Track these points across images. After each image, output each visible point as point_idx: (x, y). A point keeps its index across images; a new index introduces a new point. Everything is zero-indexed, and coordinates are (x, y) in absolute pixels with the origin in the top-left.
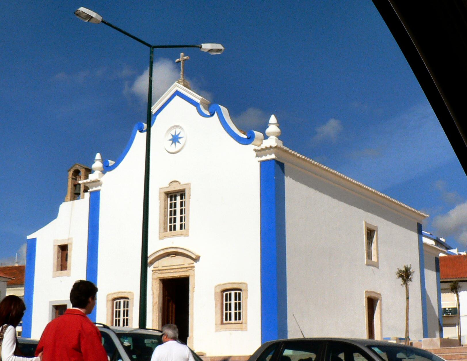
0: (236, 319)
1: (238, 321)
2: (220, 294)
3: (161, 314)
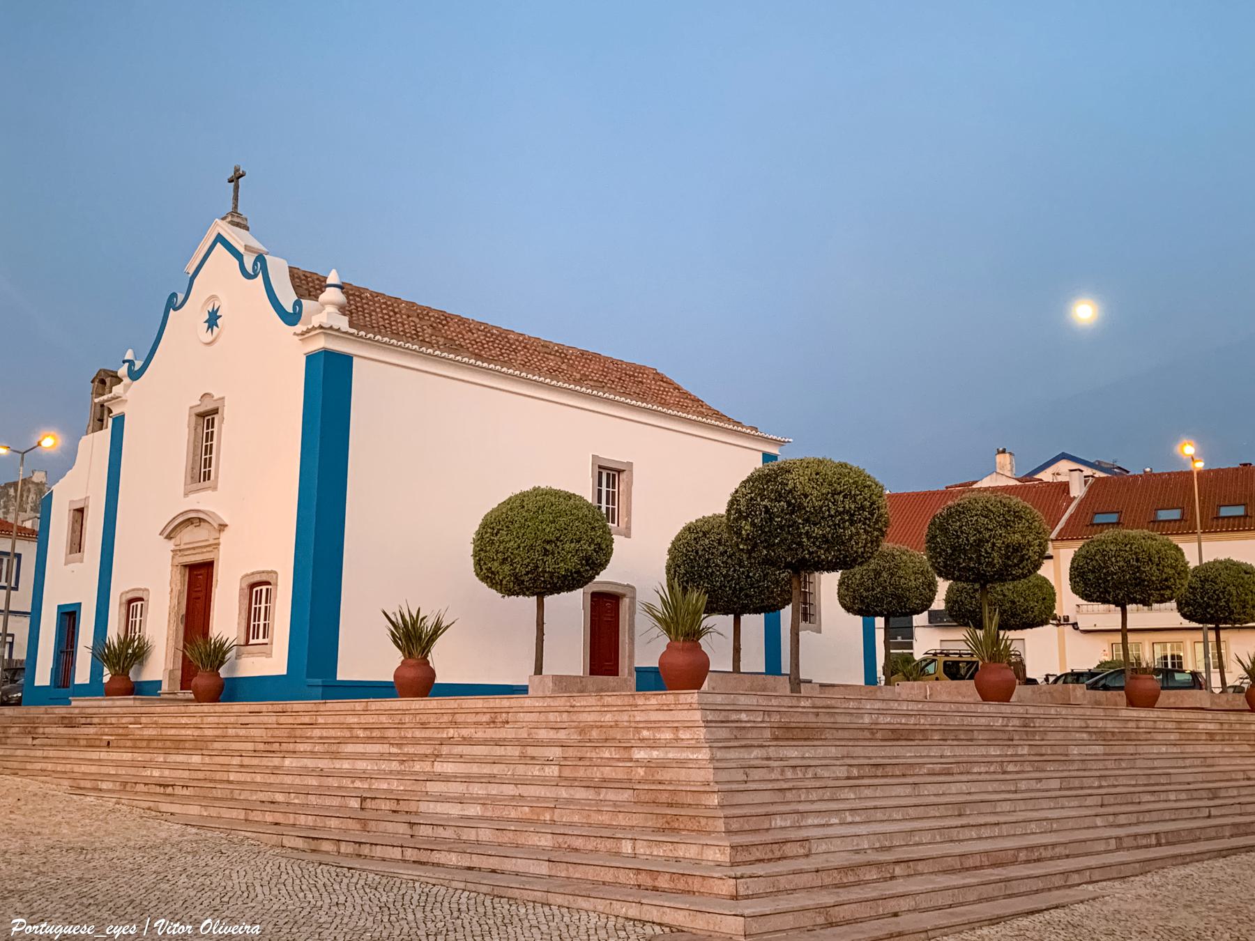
2: (247, 591)
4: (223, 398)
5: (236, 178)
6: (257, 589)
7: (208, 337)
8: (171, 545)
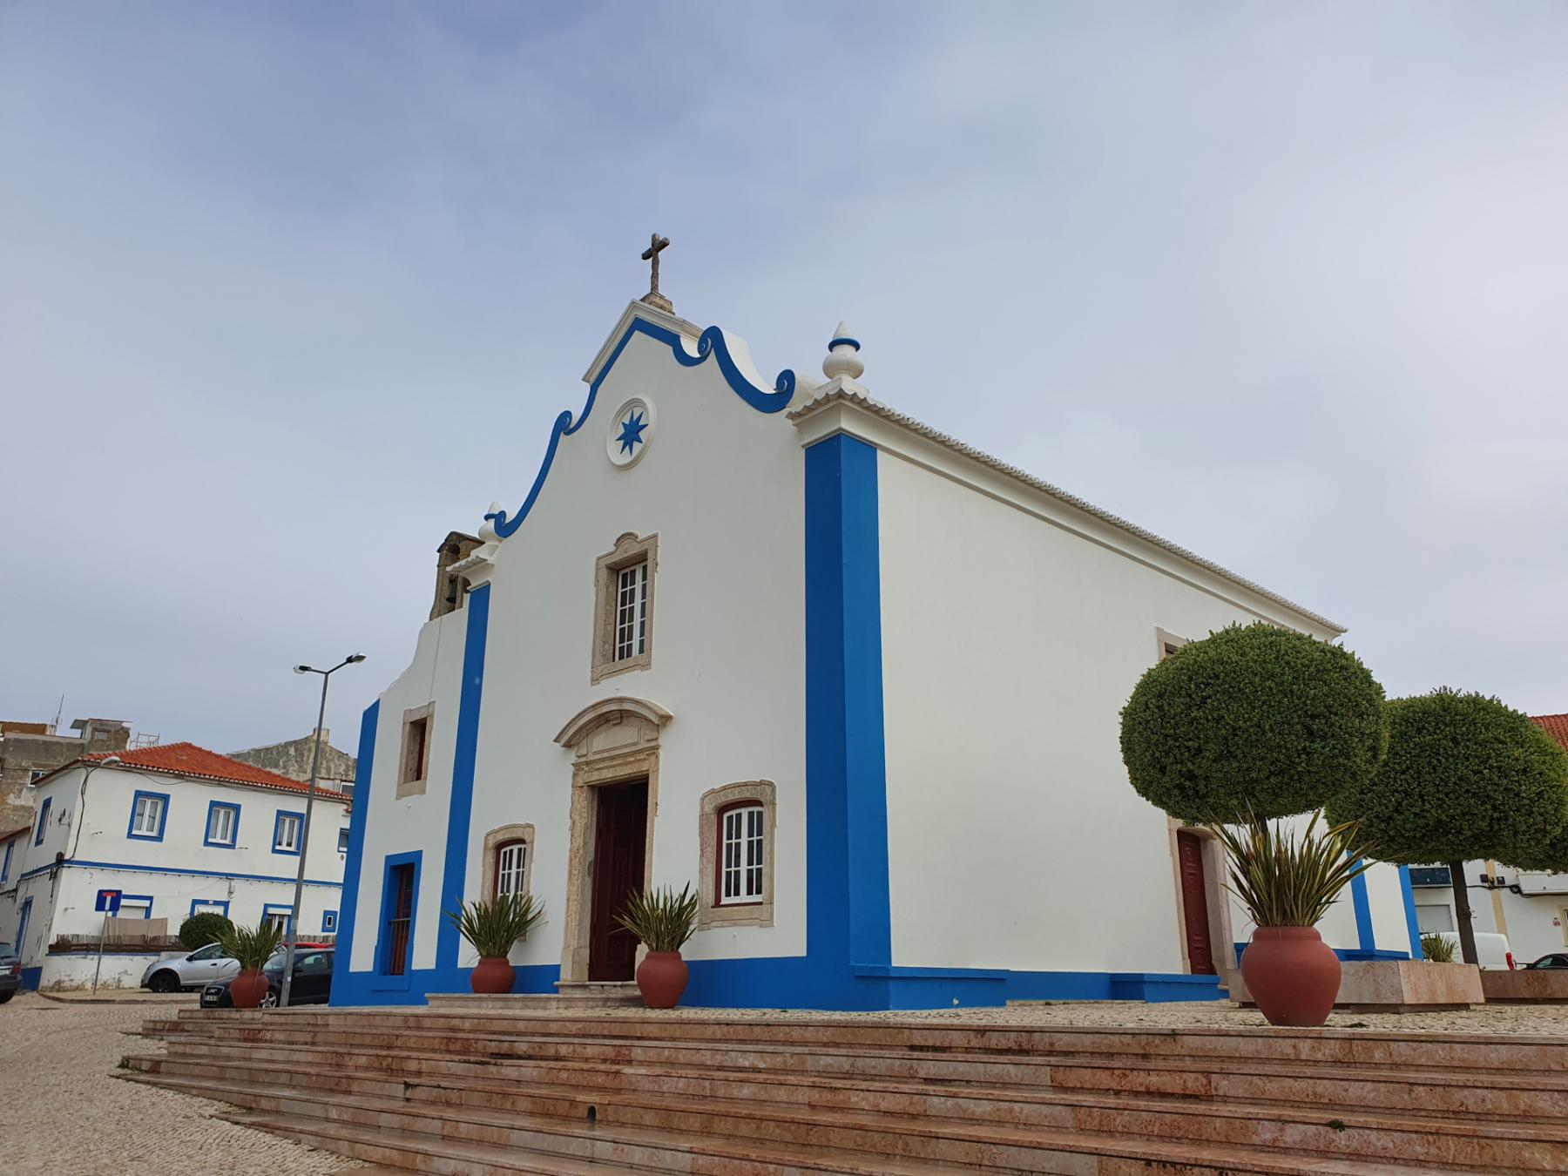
0: (750, 892)
1: (755, 898)
2: (714, 818)
3: (589, 881)
4: (655, 536)
5: (659, 245)
6: (736, 815)
7: (626, 458)
8: (572, 757)
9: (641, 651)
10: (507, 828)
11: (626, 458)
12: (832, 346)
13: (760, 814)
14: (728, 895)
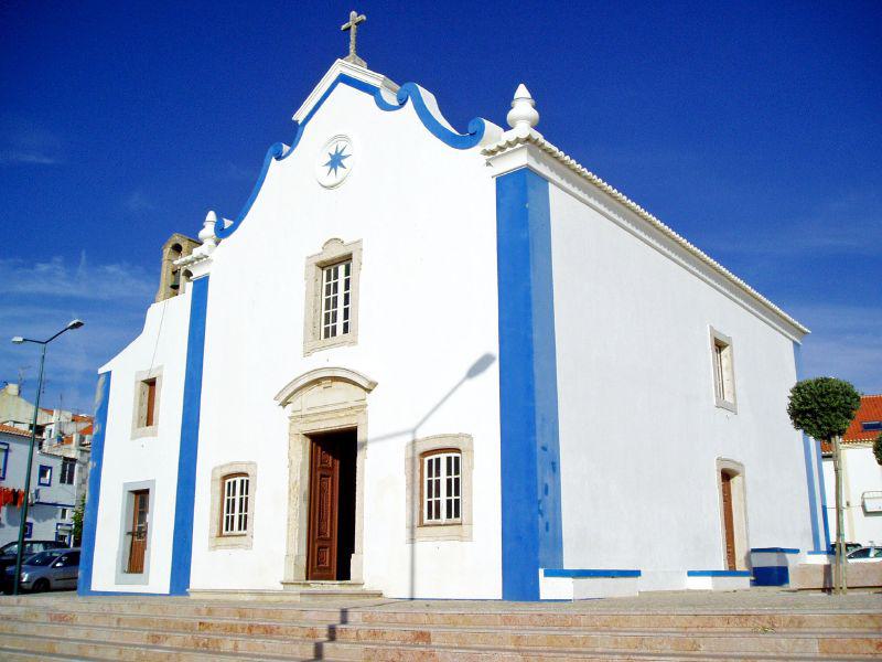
3: (305, 506)
9: (346, 330)
10: (232, 464)
11: (331, 180)
12: (732, 409)
13: (457, 459)
14: (227, 529)
